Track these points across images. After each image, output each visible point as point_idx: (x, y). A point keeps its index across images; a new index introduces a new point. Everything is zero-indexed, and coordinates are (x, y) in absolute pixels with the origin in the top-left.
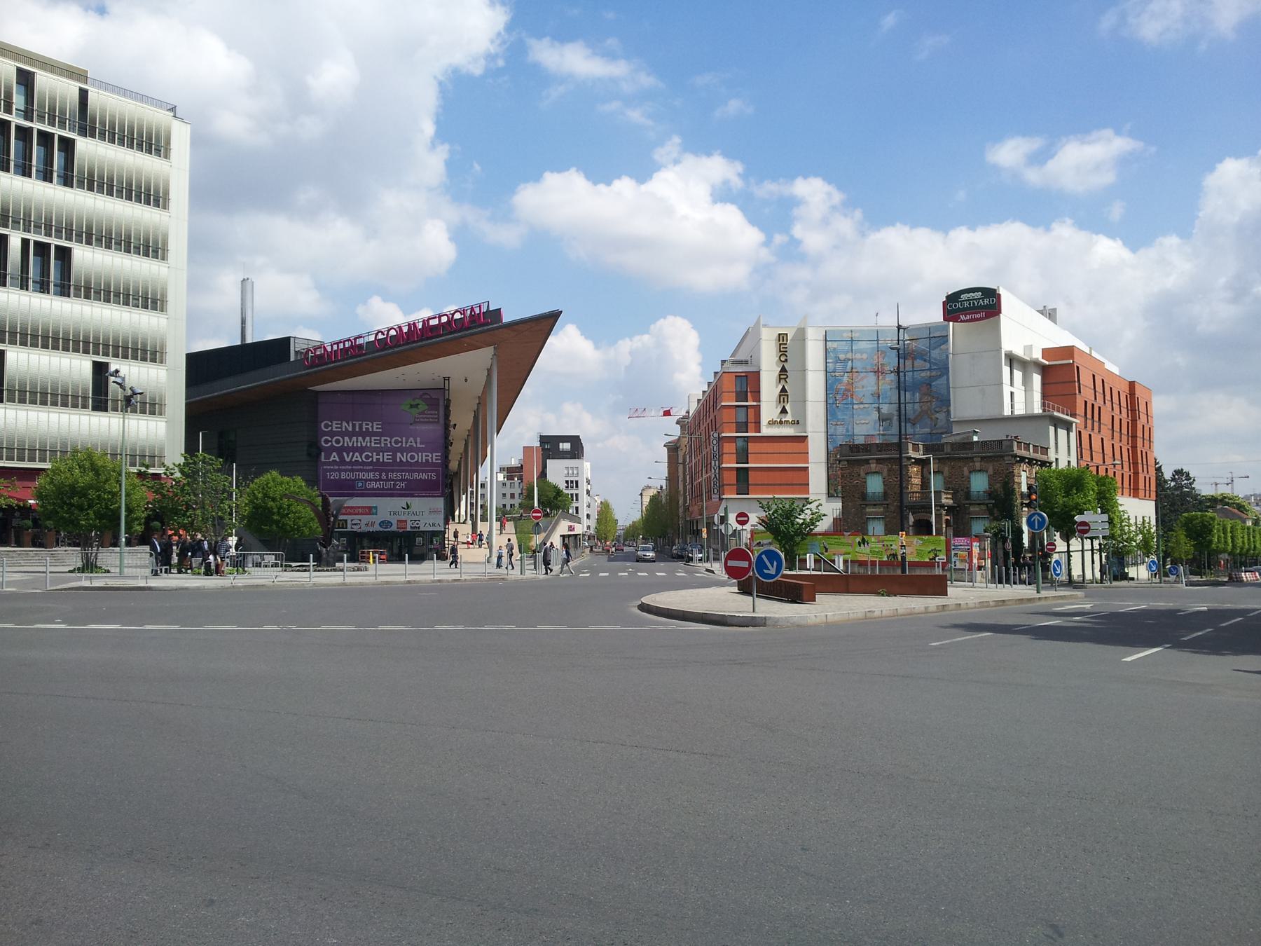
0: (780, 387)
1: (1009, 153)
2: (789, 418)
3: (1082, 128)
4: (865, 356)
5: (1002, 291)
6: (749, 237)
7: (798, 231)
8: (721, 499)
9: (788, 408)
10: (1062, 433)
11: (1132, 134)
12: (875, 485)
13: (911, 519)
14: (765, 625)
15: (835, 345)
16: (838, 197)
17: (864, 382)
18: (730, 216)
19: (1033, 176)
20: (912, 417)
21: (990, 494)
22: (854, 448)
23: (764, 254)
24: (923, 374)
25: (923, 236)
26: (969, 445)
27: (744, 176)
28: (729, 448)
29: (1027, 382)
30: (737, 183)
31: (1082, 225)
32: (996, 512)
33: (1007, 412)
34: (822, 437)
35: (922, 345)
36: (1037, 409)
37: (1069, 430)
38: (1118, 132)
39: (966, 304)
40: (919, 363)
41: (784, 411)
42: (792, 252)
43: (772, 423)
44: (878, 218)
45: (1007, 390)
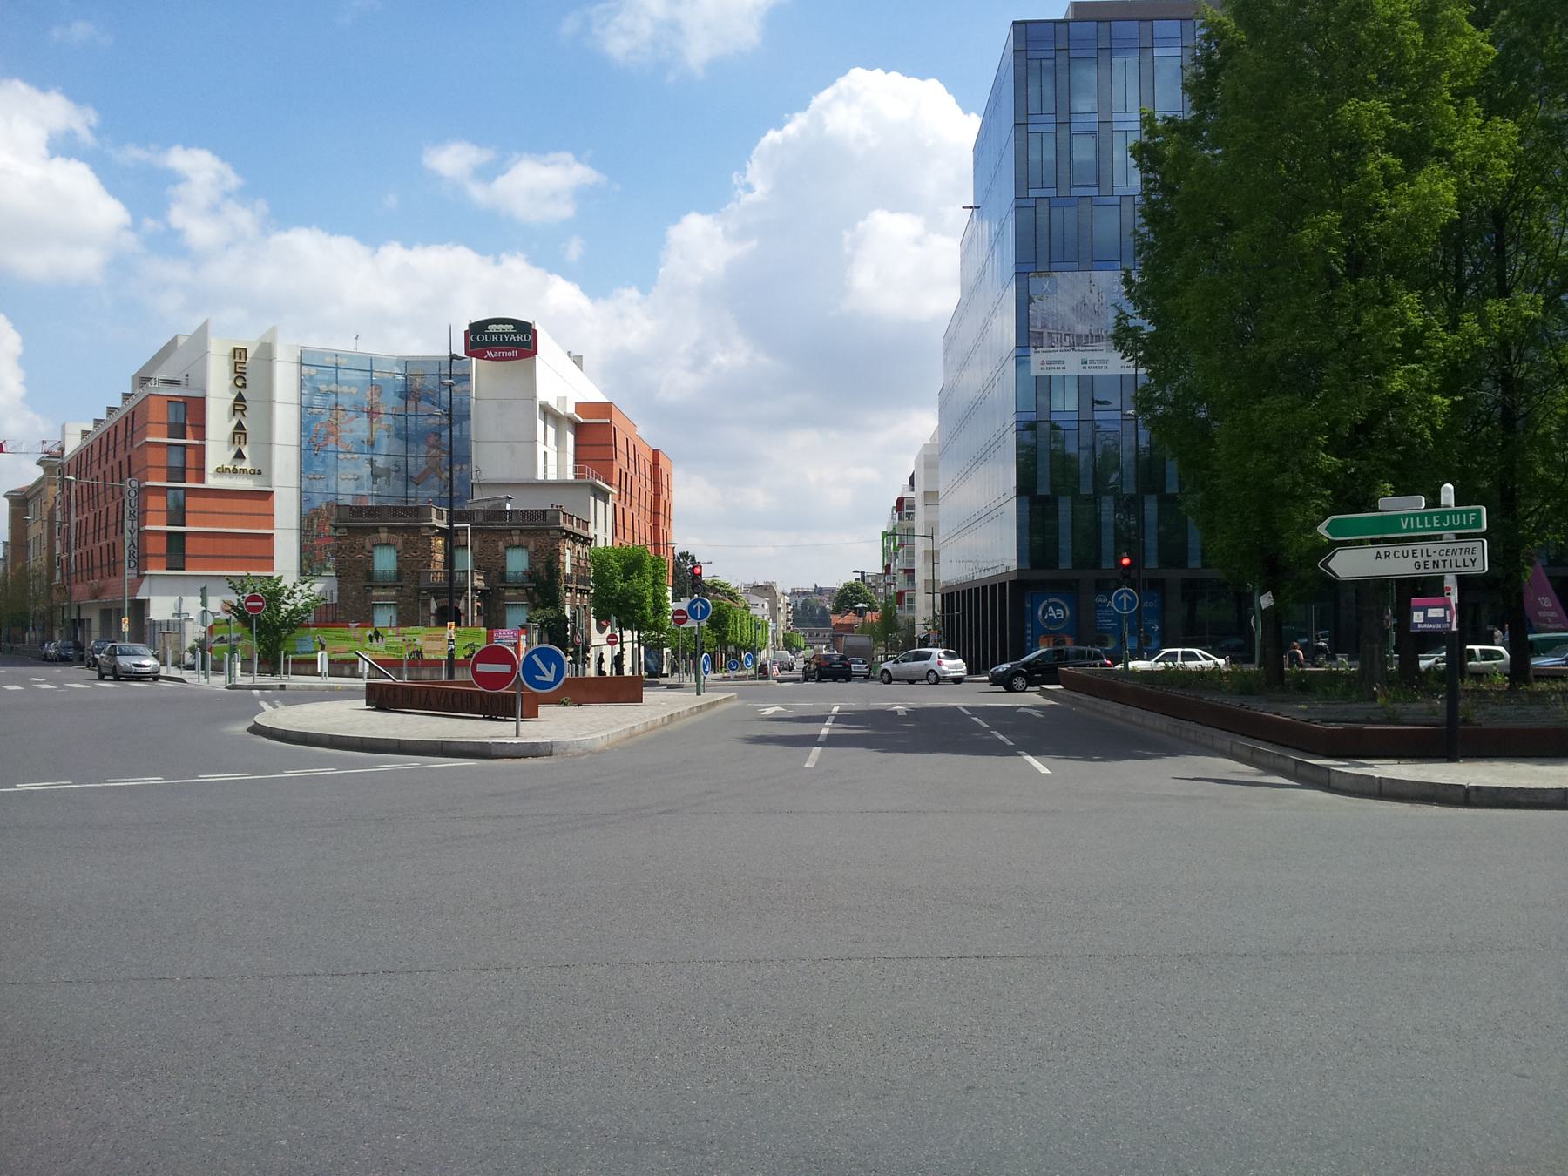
0: (235, 422)
1: (452, 160)
2: (247, 465)
3: (539, 145)
4: (354, 390)
5: (537, 327)
6: (107, 213)
7: (177, 216)
8: (141, 577)
9: (245, 451)
10: (600, 504)
11: (593, 163)
12: (385, 561)
13: (434, 606)
14: (550, 754)
15: (313, 371)
16: (234, 181)
17: (354, 424)
18: (76, 179)
19: (477, 192)
20: (416, 475)
21: (531, 575)
22: (356, 511)
23: (129, 241)
24: (431, 421)
25: (344, 248)
26: (500, 514)
27: (97, 132)
28: (155, 502)
29: (559, 440)
30: (86, 136)
31: (535, 261)
32: (537, 599)
33: (540, 477)
34: (295, 493)
35: (431, 383)
36: (570, 477)
37: (606, 502)
38: (579, 159)
39: (495, 338)
40: (424, 406)
41: (239, 455)
42: (170, 244)
43: (222, 471)
44: (284, 216)
45: (541, 449)
